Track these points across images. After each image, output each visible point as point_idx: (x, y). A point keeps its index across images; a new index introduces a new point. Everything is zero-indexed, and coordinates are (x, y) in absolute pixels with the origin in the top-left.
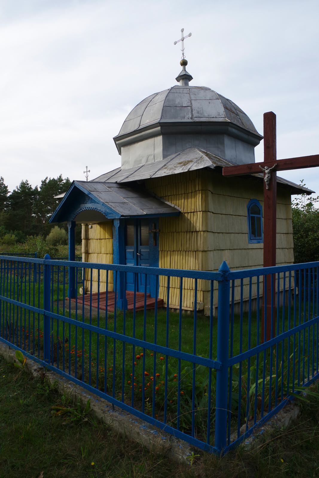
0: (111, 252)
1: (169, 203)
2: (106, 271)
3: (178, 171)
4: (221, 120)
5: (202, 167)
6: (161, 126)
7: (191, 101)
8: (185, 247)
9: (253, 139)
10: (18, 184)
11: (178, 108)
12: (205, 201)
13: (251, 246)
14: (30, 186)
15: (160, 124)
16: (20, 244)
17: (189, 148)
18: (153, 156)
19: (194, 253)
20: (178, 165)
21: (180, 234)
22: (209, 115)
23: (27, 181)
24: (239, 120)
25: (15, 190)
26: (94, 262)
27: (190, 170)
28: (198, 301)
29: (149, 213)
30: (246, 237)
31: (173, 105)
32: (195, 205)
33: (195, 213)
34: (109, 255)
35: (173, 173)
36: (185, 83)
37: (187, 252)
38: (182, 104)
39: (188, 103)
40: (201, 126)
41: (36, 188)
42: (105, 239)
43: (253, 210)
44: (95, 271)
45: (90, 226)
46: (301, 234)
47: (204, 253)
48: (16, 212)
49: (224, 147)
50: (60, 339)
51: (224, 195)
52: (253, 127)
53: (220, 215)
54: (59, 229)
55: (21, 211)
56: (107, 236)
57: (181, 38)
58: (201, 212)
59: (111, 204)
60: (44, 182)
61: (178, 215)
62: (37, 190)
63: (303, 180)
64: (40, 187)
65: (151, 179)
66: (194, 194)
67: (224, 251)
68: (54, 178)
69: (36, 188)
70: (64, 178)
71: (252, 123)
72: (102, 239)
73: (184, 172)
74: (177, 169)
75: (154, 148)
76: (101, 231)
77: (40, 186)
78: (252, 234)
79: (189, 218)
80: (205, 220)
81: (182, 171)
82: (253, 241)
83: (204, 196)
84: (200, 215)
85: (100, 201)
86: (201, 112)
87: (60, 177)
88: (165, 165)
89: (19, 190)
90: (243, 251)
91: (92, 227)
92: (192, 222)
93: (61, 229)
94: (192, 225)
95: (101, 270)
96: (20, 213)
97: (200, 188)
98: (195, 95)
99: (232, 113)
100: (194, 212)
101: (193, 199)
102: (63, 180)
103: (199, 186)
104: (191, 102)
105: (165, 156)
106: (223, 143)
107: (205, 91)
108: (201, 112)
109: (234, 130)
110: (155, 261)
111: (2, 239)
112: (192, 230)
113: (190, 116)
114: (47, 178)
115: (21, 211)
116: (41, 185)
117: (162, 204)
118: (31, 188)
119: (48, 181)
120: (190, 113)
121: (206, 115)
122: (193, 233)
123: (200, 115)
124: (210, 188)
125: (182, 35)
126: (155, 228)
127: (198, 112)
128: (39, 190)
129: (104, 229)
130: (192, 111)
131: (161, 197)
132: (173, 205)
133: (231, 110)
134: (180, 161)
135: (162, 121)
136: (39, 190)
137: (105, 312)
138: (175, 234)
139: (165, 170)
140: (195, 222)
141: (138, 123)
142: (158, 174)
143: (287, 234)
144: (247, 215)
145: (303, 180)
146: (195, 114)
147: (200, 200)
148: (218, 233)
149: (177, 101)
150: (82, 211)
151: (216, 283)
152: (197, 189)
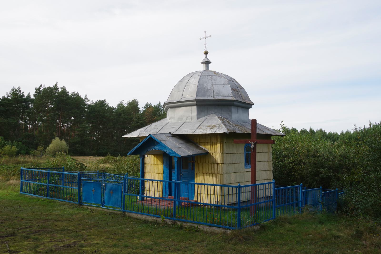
0: (162, 172)
1: (201, 147)
2: (228, 187)
3: (209, 132)
4: (230, 98)
5: (222, 132)
6: (196, 101)
7: (213, 85)
8: (211, 171)
9: (247, 106)
10: (9, 91)
11: (205, 90)
12: (222, 148)
13: (246, 170)
14: (23, 93)
15: (196, 100)
16: (21, 155)
17: (212, 114)
18: (190, 117)
19: (216, 175)
20: (208, 128)
21: (208, 164)
22: (223, 95)
23: (20, 88)
24: (240, 95)
25: (4, 96)
26: (149, 178)
27: (216, 133)
28: (219, 201)
29: (193, 154)
30: (243, 165)
31: (203, 88)
33: (217, 153)
34: (160, 174)
35: (206, 133)
36: (207, 66)
37: (212, 174)
38: (208, 87)
39: (211, 86)
40: (219, 101)
41: (29, 96)
42: (158, 164)
43: (248, 148)
44: (242, 188)
45: (146, 155)
46: (281, 159)
47: (222, 175)
48: (7, 120)
49: (231, 113)
51: (231, 143)
52: (248, 98)
53: (229, 154)
54: (59, 140)
55: (12, 119)
56: (159, 162)
57: (204, 36)
58: (220, 153)
59: (174, 149)
60: (38, 91)
61: (207, 154)
62: (30, 97)
63: (283, 121)
64: (34, 95)
65: (193, 134)
66: (216, 143)
67: (232, 174)
68: (49, 86)
69: (29, 96)
70: (60, 86)
71: (248, 95)
72: (155, 164)
73: (212, 134)
74: (207, 130)
75: (191, 112)
76: (155, 159)
77: (34, 93)
78: (247, 163)
79: (213, 156)
80: (222, 158)
81: (211, 133)
82: (247, 167)
83: (222, 145)
84: (219, 155)
86: (219, 93)
87: (56, 85)
88: (200, 126)
89: (10, 97)
90: (242, 173)
91: (148, 156)
92: (215, 158)
93: (61, 140)
94: (215, 160)
95: (233, 188)
96: (12, 122)
97: (220, 141)
98: (215, 80)
99: (236, 92)
100: (216, 153)
101: (213, 146)
102: (58, 88)
103: (220, 137)
104: (213, 86)
105: (198, 118)
107: (220, 78)
108: (219, 93)
109: (237, 103)
110: (193, 178)
111: (3, 150)
112: (215, 162)
113: (213, 95)
114: (41, 86)
115: (12, 119)
116: (35, 92)
117: (198, 147)
118: (23, 95)
119: (42, 89)
120: (212, 94)
122: (216, 164)
123: (218, 95)
124: (225, 141)
125: (205, 35)
127: (217, 93)
128: (32, 97)
129: (157, 158)
130: (213, 92)
131: (196, 143)
132: (204, 148)
133: (236, 90)
134: (209, 125)
135: (197, 99)
136: (32, 97)
137: (167, 207)
138: (205, 164)
139: (201, 130)
140: (216, 158)
141: (181, 95)
142: (197, 131)
143: (268, 162)
144: (244, 152)
145: (283, 121)
146: (215, 94)
147: (220, 147)
148: (228, 164)
149: (205, 85)
150: (152, 150)
151: (237, 188)
152: (218, 141)
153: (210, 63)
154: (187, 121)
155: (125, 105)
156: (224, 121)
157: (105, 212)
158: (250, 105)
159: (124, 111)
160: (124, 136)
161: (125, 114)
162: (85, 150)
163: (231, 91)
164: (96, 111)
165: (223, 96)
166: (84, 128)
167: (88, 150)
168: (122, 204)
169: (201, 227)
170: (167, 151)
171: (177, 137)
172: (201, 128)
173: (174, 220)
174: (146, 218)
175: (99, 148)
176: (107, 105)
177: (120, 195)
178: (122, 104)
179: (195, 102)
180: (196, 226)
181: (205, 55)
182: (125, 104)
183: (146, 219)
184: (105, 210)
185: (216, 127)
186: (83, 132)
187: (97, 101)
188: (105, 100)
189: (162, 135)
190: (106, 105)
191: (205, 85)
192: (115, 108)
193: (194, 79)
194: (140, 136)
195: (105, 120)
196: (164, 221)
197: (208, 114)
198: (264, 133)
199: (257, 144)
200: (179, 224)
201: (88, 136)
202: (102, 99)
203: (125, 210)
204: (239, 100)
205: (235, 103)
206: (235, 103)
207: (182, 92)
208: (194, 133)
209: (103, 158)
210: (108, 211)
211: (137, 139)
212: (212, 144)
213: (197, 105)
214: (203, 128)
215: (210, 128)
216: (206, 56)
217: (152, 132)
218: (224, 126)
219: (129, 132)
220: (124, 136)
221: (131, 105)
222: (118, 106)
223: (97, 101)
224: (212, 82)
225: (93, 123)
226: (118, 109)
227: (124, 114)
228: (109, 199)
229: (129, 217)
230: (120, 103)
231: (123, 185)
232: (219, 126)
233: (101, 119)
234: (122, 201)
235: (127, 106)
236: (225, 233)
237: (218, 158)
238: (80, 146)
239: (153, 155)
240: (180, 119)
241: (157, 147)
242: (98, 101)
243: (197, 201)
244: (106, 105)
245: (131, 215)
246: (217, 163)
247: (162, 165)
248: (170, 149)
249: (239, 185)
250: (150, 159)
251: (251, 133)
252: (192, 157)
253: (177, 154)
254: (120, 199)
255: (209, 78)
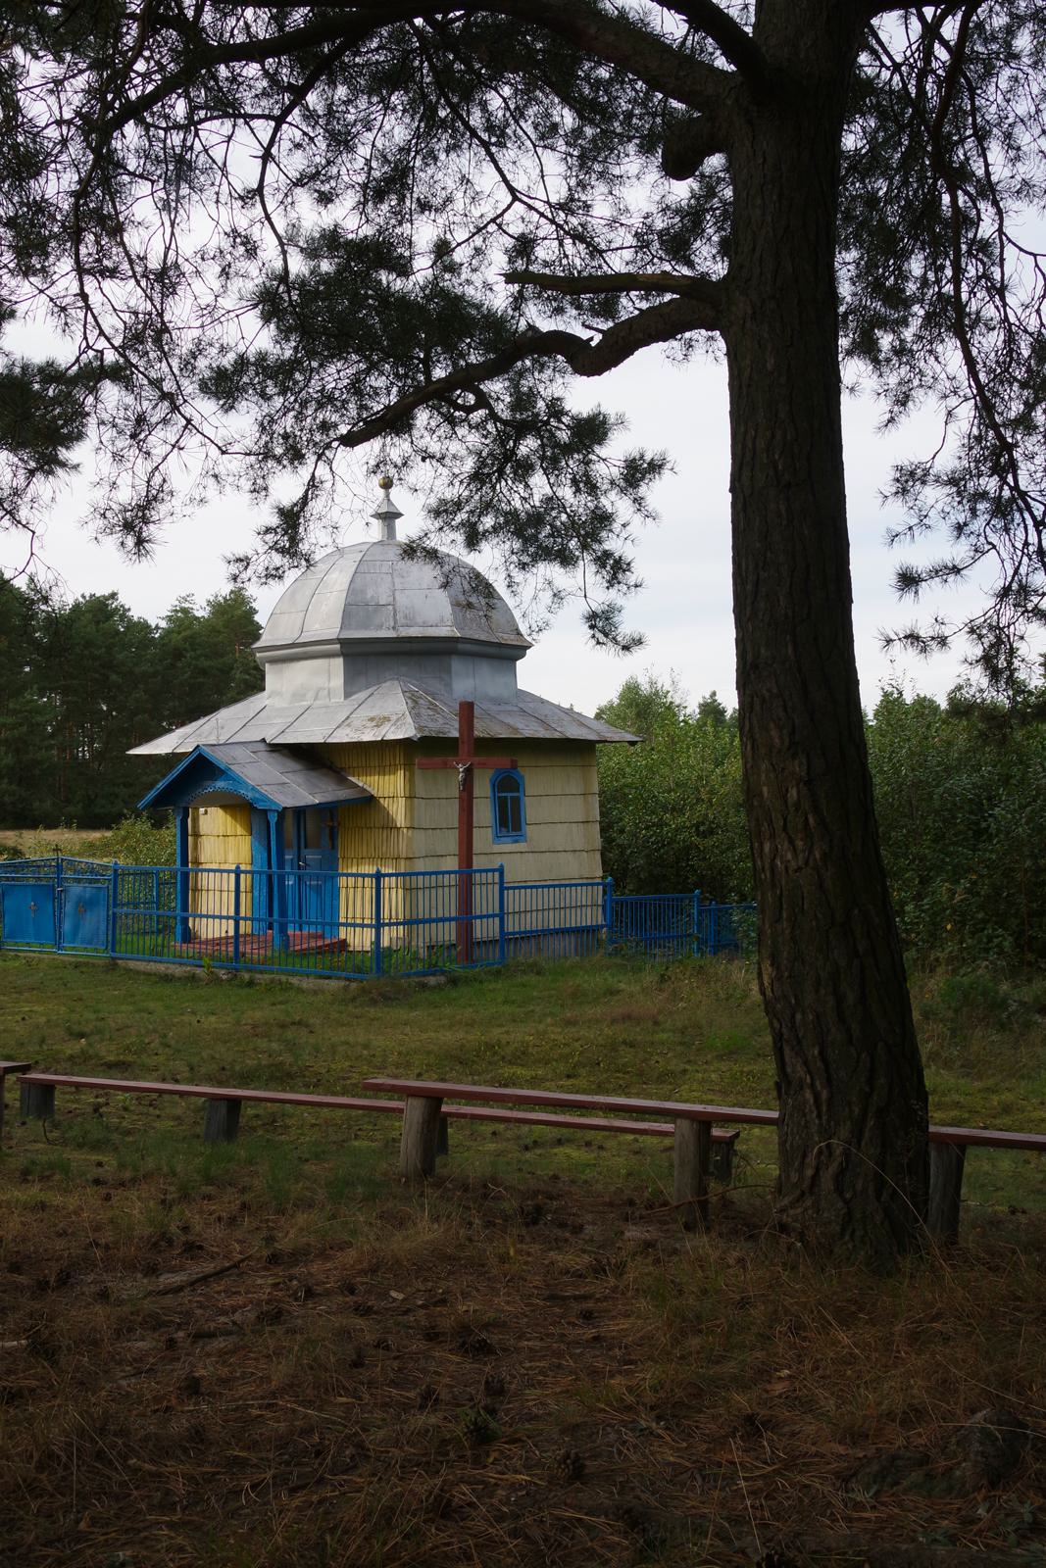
1: (354, 779)
3: (368, 736)
4: (444, 632)
11: (370, 608)
12: (410, 782)
13: (497, 848)
15: (339, 641)
18: (326, 692)
29: (324, 800)
32: (395, 787)
45: (202, 810)
47: (408, 862)
50: (992, 211)
56: (240, 830)
61: (369, 801)
65: (325, 743)
80: (410, 810)
81: (374, 739)
85: (246, 783)
91: (206, 812)
101: (387, 777)
105: (347, 695)
106: (449, 671)
113: (392, 624)
121: (420, 621)
126: (332, 820)
129: (234, 817)
130: (395, 611)
132: (361, 784)
134: (372, 715)
139: (348, 730)
149: (370, 593)
153: (399, 515)
154: (318, 702)
155: (199, 614)
156: (421, 701)
157: (63, 962)
158: (520, 650)
159: (193, 641)
160: (131, 752)
161: (199, 652)
162: (36, 804)
163: (448, 609)
164: (79, 644)
165: (425, 625)
166: (30, 712)
167: (49, 803)
168: (110, 938)
169: (294, 981)
170: (250, 795)
171: (286, 751)
172: (349, 725)
173: (237, 970)
174: (167, 968)
175: (96, 796)
176: (123, 616)
177: (103, 914)
178: (185, 611)
179: (338, 646)
180: (284, 978)
181: (382, 491)
182: (201, 611)
183: (170, 971)
184: (66, 958)
185: (389, 720)
186: (25, 728)
187: (81, 600)
188: (113, 596)
189: (236, 746)
190: (121, 616)
191: (370, 593)
192: (157, 627)
193: (341, 571)
194: (178, 751)
195: (114, 677)
196: (212, 972)
197: (379, 682)
198: (557, 735)
199: (476, 772)
200: (246, 976)
201: (51, 747)
202: (101, 591)
203: (117, 955)
204: (476, 637)
205: (460, 646)
206: (460, 646)
207: (302, 614)
208: (329, 741)
209: (109, 834)
210: (73, 960)
211: (173, 758)
212: (383, 770)
213: (343, 654)
214: (357, 723)
215: (374, 724)
216: (388, 495)
217: (202, 741)
218: (409, 720)
219: (139, 744)
220: (131, 752)
221: (223, 614)
222: (169, 619)
223: (81, 600)
224: (394, 583)
225: (65, 691)
226: (167, 632)
227: (194, 650)
228: (76, 929)
229: (125, 969)
230: (177, 603)
231: (111, 887)
232: (398, 720)
233: (97, 676)
234: (110, 932)
235: (207, 620)
236: (346, 988)
237: (398, 811)
238: (13, 787)
239: (221, 807)
240: (298, 696)
241: (220, 784)
242: (83, 597)
243: (345, 940)
244: (121, 616)
245: (132, 964)
246: (396, 828)
247: (248, 839)
248: (253, 788)
249: (378, 872)
250: (213, 822)
251: (456, 734)
252: (327, 812)
253: (272, 801)
254: (103, 927)
255: (384, 570)
